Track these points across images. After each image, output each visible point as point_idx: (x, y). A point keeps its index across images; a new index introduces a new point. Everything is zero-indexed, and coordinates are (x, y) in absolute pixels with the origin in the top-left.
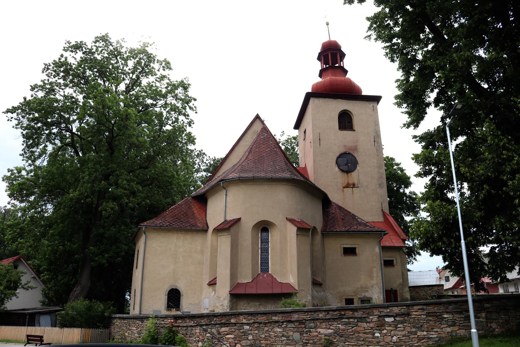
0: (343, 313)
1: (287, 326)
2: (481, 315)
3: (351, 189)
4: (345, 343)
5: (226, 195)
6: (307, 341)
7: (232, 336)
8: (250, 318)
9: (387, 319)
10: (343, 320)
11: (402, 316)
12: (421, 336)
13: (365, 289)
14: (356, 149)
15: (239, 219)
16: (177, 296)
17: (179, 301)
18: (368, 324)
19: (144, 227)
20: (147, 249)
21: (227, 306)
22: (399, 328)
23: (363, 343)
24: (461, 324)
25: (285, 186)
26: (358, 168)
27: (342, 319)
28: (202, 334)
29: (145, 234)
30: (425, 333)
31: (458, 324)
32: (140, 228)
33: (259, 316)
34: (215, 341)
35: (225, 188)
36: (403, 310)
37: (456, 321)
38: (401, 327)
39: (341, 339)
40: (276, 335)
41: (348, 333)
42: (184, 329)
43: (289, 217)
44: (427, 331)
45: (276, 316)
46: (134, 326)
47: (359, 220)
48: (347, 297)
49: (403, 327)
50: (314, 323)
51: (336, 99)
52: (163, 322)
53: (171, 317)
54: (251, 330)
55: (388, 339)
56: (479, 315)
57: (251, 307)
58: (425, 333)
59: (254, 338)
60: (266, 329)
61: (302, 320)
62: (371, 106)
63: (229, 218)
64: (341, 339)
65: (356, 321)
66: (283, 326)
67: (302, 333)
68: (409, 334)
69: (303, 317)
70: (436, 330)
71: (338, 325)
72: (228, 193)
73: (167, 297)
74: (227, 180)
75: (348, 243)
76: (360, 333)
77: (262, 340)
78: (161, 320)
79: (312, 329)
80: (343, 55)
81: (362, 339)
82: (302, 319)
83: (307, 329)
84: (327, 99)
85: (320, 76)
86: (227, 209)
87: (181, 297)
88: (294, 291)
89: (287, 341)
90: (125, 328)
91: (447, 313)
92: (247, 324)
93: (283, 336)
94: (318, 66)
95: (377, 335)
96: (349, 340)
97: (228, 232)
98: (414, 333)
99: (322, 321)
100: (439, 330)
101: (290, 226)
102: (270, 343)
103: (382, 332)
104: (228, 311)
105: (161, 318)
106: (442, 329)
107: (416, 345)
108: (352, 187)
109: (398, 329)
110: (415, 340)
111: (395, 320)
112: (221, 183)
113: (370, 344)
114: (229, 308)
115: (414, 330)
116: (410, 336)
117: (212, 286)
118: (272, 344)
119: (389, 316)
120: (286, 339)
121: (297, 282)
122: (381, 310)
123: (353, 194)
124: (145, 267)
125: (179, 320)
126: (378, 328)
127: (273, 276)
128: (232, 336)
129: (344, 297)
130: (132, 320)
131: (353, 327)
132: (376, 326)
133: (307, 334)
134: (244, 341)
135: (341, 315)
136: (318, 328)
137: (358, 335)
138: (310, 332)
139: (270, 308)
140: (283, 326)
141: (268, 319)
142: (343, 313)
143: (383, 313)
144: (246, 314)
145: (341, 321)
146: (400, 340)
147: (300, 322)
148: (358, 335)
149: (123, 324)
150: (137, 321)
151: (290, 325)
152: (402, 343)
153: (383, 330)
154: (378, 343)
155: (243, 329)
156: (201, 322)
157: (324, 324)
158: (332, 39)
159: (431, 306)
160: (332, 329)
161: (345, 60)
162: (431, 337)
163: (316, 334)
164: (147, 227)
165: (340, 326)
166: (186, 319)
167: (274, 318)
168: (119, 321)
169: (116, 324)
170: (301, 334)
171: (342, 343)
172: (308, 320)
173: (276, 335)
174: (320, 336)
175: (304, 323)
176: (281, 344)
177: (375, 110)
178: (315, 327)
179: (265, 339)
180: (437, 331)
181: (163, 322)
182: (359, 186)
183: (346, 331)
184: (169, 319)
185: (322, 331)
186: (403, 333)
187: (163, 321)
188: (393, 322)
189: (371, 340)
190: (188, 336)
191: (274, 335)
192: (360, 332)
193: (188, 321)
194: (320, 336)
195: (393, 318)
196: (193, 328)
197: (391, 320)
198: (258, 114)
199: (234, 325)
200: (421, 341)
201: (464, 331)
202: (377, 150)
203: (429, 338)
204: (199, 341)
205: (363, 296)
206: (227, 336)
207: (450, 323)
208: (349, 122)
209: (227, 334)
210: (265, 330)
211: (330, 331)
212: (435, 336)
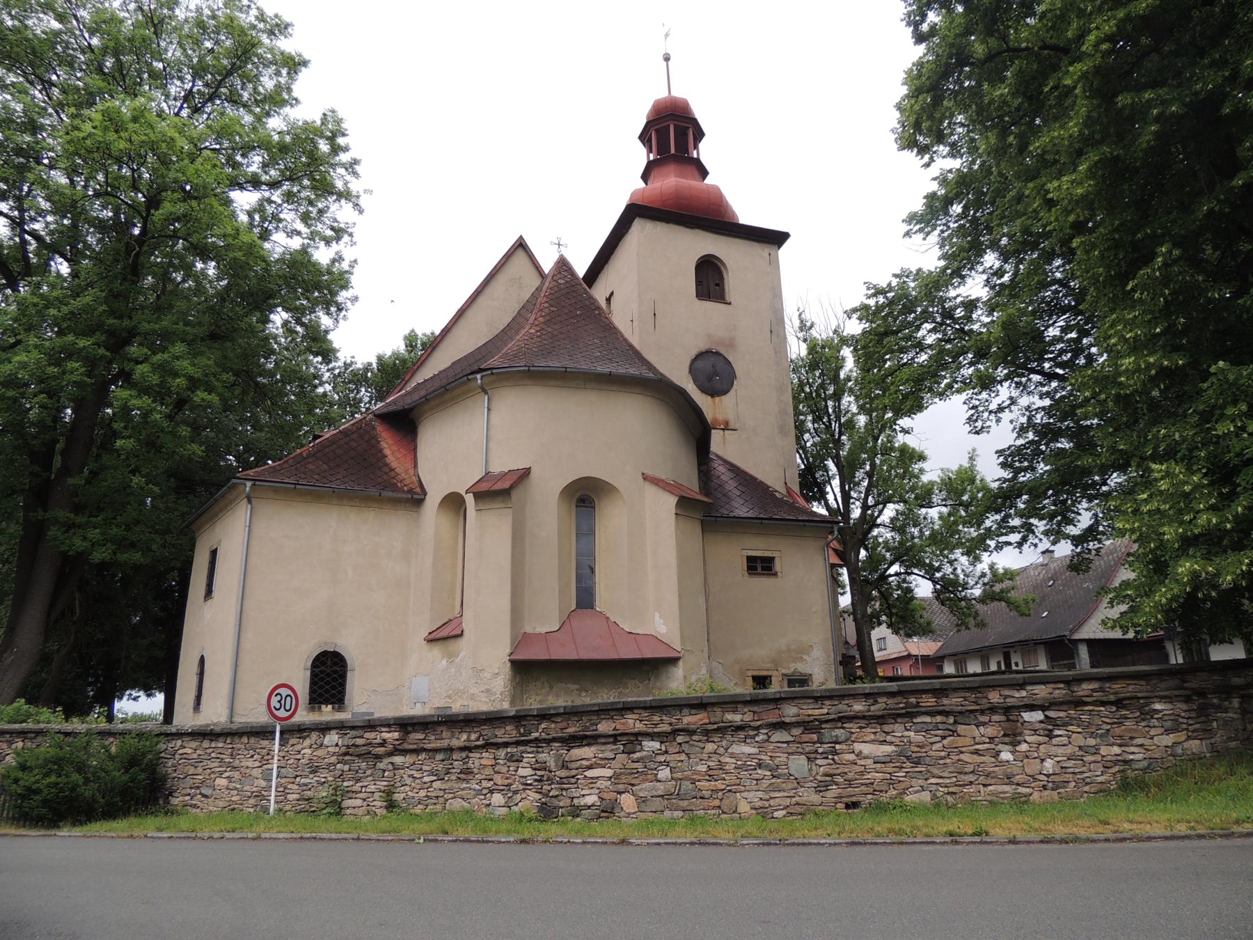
0: (913, 700)
1: (769, 737)
2: (1230, 703)
3: (721, 432)
4: (926, 780)
5: (489, 409)
6: (827, 778)
7: (608, 772)
8: (656, 718)
9: (1027, 716)
10: (919, 720)
11: (1065, 707)
12: (1109, 758)
13: (801, 651)
14: (731, 344)
15: (526, 473)
16: (336, 672)
17: (343, 685)
18: (981, 728)
19: (249, 484)
20: (254, 543)
21: (501, 694)
22: (1057, 739)
23: (971, 778)
24: (1191, 725)
25: (640, 397)
26: (735, 386)
27: (915, 717)
28: (504, 769)
29: (249, 501)
30: (1116, 750)
31: (1184, 726)
32: (235, 485)
33: (686, 711)
34: (549, 788)
35: (486, 393)
36: (1057, 691)
37: (1181, 720)
38: (1060, 736)
39: (917, 769)
40: (739, 763)
41: (933, 753)
42: (440, 756)
43: (649, 472)
44: (1120, 746)
45: (735, 711)
46: (252, 756)
47: (777, 494)
48: (756, 673)
49: (1066, 736)
50: (843, 728)
51: (691, 228)
52: (359, 741)
53: (389, 726)
54: (666, 752)
55: (1033, 767)
56: (1226, 703)
57: (558, 696)
58: (1116, 750)
59: (675, 775)
60: (710, 747)
61: (811, 722)
62: (766, 254)
63: (497, 467)
64: (917, 769)
65: (951, 720)
66: (757, 739)
67: (812, 756)
68: (1081, 753)
69: (810, 712)
70: (1139, 741)
71: (906, 733)
72: (493, 403)
73: (308, 673)
74: (494, 371)
75: (759, 546)
76: (962, 752)
77: (699, 781)
78: (353, 733)
79: (839, 743)
80: (699, 134)
81: (970, 768)
82: (812, 718)
83: (826, 746)
84: (672, 226)
85: (645, 177)
86: (491, 445)
87: (349, 674)
88: (675, 655)
89: (773, 781)
90: (216, 764)
91: (1162, 698)
92: (652, 736)
93: (760, 765)
94: (640, 156)
95: (1006, 756)
96: (935, 771)
97: (503, 501)
98: (1093, 750)
99: (863, 723)
100: (1147, 742)
101: (651, 491)
102: (723, 787)
103: (1018, 748)
104: (506, 705)
105: (353, 728)
106: (1152, 738)
107: (1100, 779)
108: (723, 429)
109: (1055, 741)
110: (1098, 768)
111: (1046, 716)
112: (479, 376)
113: (989, 781)
114: (508, 699)
115: (1091, 742)
116: (1085, 759)
117: (439, 643)
118: (730, 791)
119: (1031, 708)
120: (769, 773)
121: (677, 633)
122: (1006, 692)
123: (724, 443)
124: (245, 594)
125: (415, 731)
126: (1007, 739)
127: (608, 618)
128: (608, 773)
129: (750, 673)
130: (245, 740)
131: (944, 738)
132: (1002, 733)
133: (827, 758)
134: (644, 786)
135: (908, 705)
136: (853, 742)
137: (957, 757)
138: (835, 753)
139: (605, 697)
140: (757, 739)
141: (713, 720)
142: (913, 700)
143: (1012, 700)
144: (645, 708)
145: (915, 721)
146: (1062, 768)
147: (808, 725)
148: (957, 757)
149: (208, 751)
150: (261, 742)
151: (778, 736)
152: (1067, 776)
153: (1019, 743)
154: (1008, 778)
155: (642, 750)
156: (496, 736)
157: (869, 730)
158: (678, 93)
159: (1119, 682)
160: (891, 743)
161: (702, 145)
162: (1132, 760)
163: (852, 757)
164: (257, 483)
165: (912, 734)
166: (440, 729)
167: (729, 717)
168: (194, 744)
169: (180, 752)
170: (809, 759)
171: (920, 781)
172: (827, 721)
173: (739, 763)
174: (862, 762)
175: (817, 730)
176: (756, 788)
177: (774, 263)
178: (846, 741)
179: (707, 777)
180: (1141, 745)
181: (359, 741)
182: (737, 426)
183: (927, 749)
184: (383, 729)
185: (866, 749)
186: (1069, 750)
187: (362, 737)
188: (1041, 722)
189: (991, 769)
190: (453, 777)
191: (734, 766)
192: (963, 749)
193: (446, 734)
194: (862, 762)
195: (1040, 712)
196: (471, 755)
197: (1037, 716)
198: (521, 237)
199: (611, 740)
200: (1110, 771)
201: (1197, 742)
202: (776, 353)
203: (1126, 762)
204: (491, 792)
205: (792, 670)
206: (590, 773)
207: (1168, 724)
208: (717, 285)
209: (589, 768)
210: (705, 750)
211: (889, 749)
212: (1140, 756)
